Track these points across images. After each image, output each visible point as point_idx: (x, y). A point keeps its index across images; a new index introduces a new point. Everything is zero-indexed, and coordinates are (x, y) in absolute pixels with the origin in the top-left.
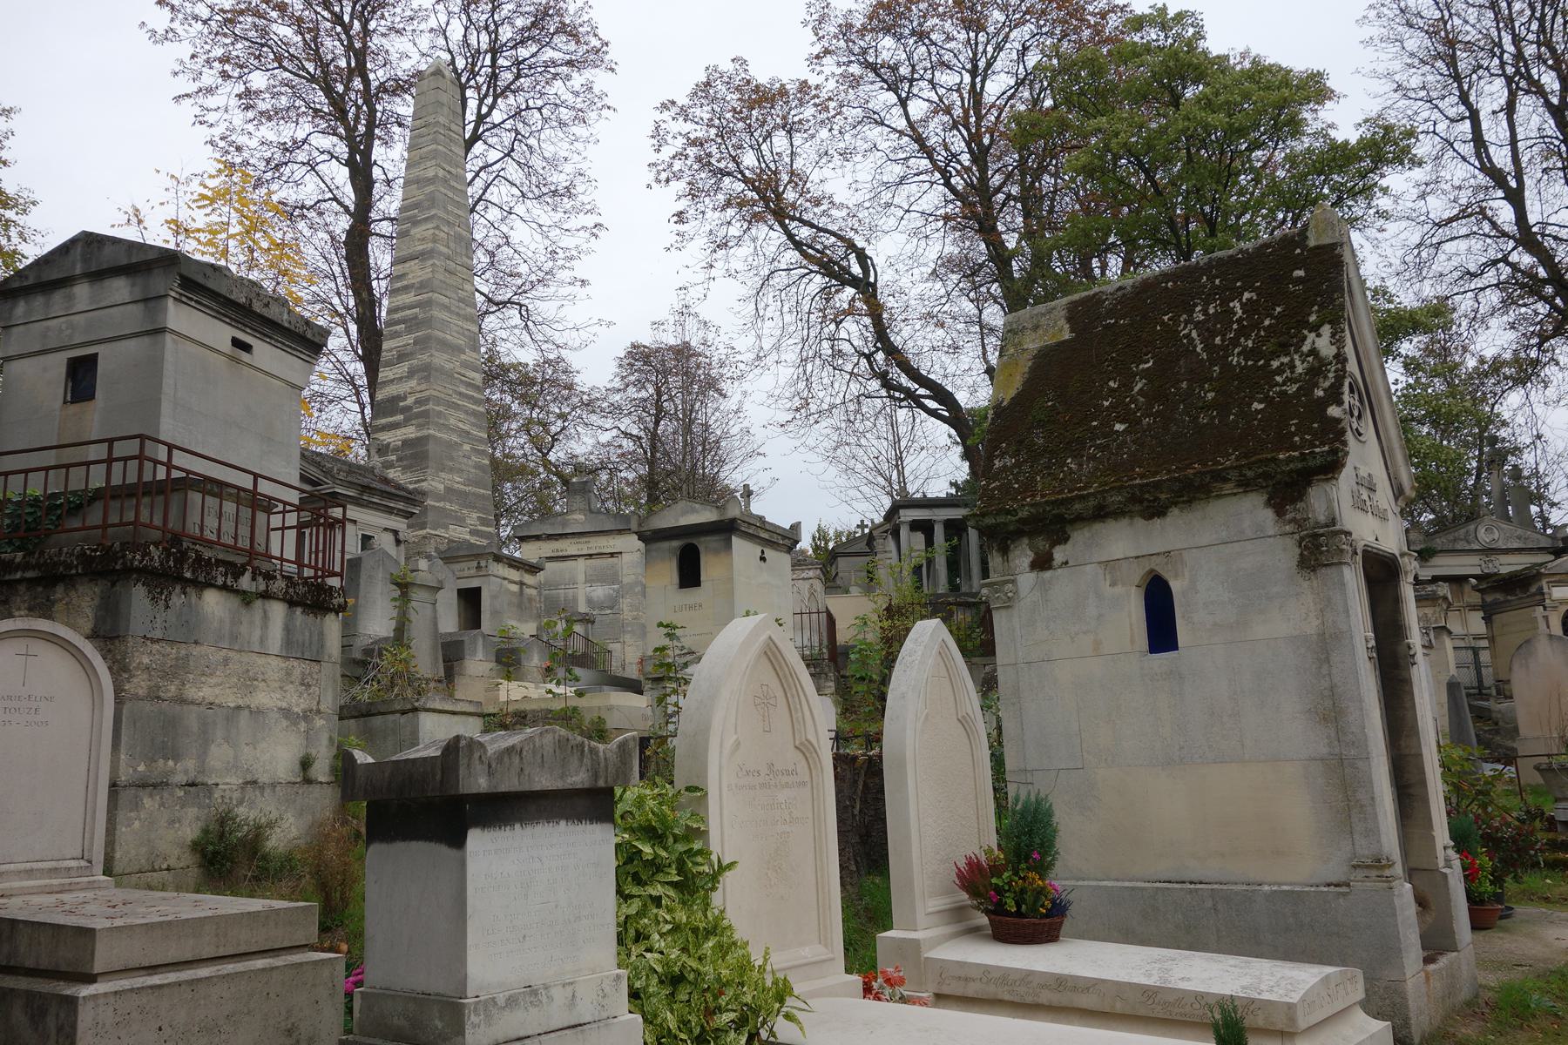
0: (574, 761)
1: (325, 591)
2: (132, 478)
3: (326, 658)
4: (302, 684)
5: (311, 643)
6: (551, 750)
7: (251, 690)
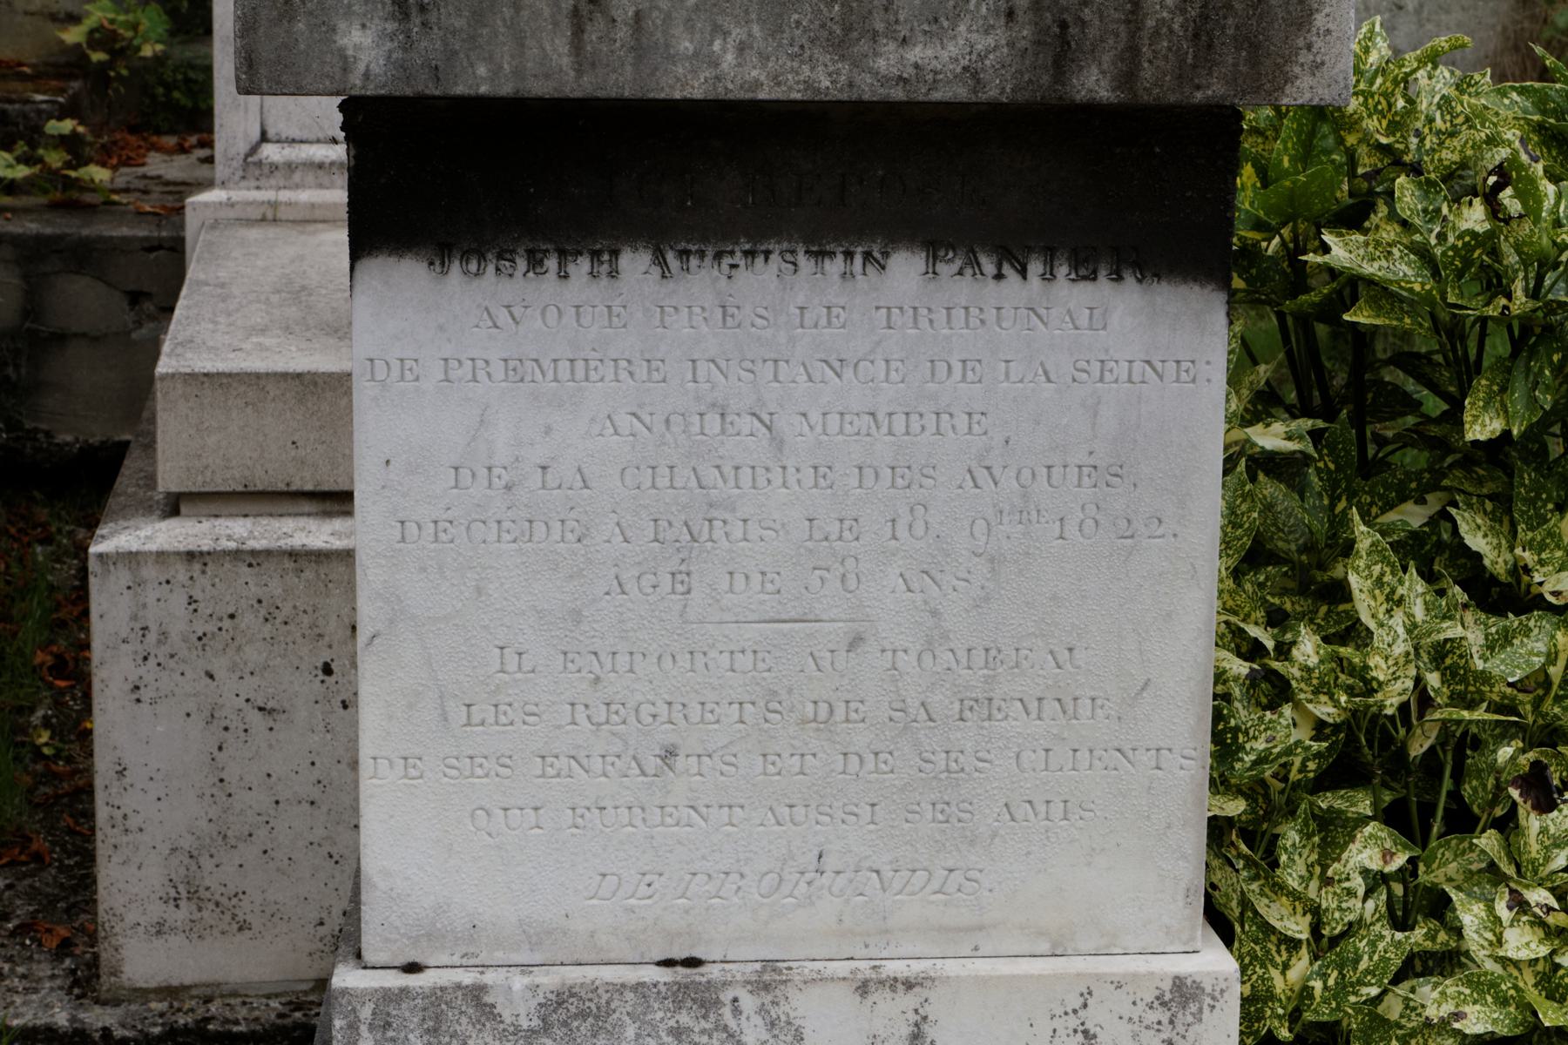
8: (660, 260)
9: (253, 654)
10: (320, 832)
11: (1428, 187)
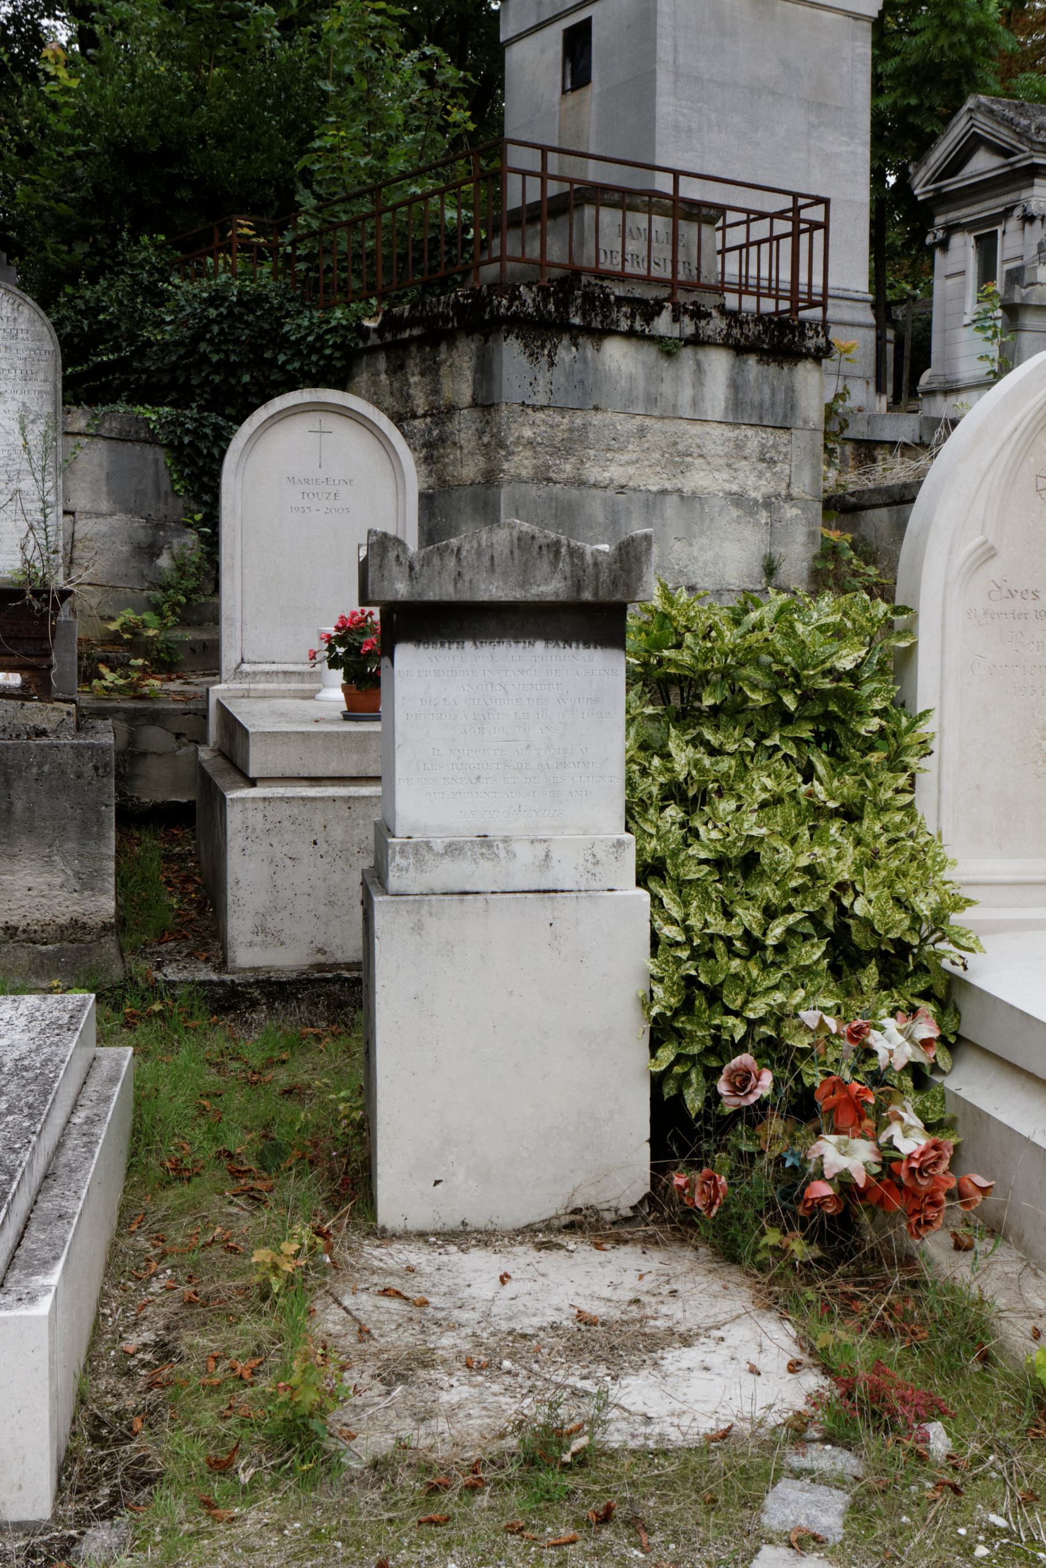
0: (544, 566)
1: (792, 329)
2: (534, 195)
3: (800, 423)
4: (763, 460)
5: (773, 404)
6: (507, 551)
7: (683, 469)
8: (475, 643)
9: (288, 837)
10: (311, 907)
11: (696, 636)
